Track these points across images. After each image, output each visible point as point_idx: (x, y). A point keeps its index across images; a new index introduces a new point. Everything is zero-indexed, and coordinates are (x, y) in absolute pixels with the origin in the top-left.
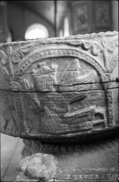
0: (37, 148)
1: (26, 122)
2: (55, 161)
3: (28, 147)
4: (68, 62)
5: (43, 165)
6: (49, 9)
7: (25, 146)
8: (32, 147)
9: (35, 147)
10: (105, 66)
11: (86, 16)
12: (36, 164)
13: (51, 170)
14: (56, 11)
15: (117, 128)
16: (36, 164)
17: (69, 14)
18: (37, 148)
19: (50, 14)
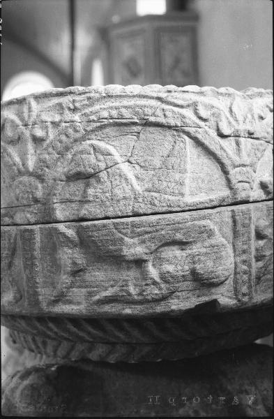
6: (58, 39)
14: (73, 47)
17: (103, 53)
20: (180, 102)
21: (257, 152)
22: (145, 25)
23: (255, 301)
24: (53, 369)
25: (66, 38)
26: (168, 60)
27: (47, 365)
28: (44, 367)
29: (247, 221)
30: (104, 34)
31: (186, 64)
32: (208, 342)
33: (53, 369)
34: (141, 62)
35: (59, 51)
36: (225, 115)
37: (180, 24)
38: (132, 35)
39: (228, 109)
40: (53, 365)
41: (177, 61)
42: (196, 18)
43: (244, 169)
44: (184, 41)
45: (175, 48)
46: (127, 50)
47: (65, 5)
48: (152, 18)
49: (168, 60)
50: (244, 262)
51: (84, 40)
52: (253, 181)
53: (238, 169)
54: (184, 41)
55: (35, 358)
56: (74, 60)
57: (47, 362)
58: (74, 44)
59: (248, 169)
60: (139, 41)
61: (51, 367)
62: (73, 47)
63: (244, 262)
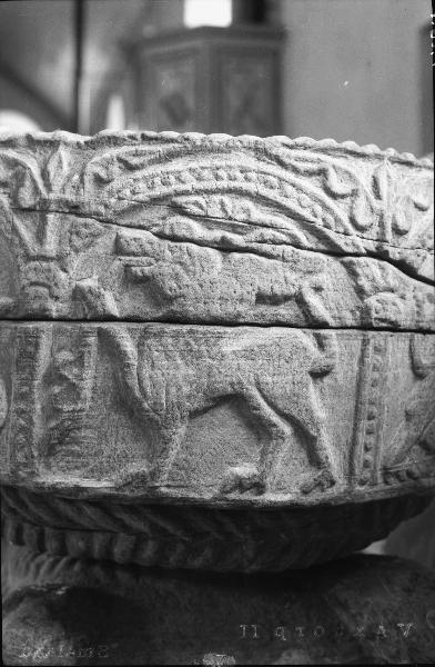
0: (28, 568)
6: (53, 60)
14: (78, 73)
17: (127, 86)
18: (28, 568)
20: (302, 166)
21: (74, 237)
22: (198, 43)
23: (40, 480)
24: (60, 593)
25: (66, 60)
26: (234, 100)
27: (48, 585)
28: (45, 590)
29: (31, 349)
30: (134, 58)
31: (262, 107)
32: (301, 556)
33: (60, 593)
34: (190, 101)
35: (57, 79)
36: (34, 181)
37: (258, 43)
38: (176, 58)
39: (371, 180)
40: (59, 587)
41: (248, 103)
42: (280, 35)
43: (44, 264)
44: (261, 72)
45: (246, 80)
46: (168, 82)
47: (68, 8)
48: (208, 32)
49: (234, 100)
50: (21, 413)
51: (97, 63)
52: (56, 284)
53: (33, 264)
54: (261, 72)
55: (26, 573)
56: (80, 101)
57: (47, 581)
58: (76, 68)
59: (53, 265)
60: (188, 68)
61: (56, 590)
62: (78, 73)
63: (21, 413)
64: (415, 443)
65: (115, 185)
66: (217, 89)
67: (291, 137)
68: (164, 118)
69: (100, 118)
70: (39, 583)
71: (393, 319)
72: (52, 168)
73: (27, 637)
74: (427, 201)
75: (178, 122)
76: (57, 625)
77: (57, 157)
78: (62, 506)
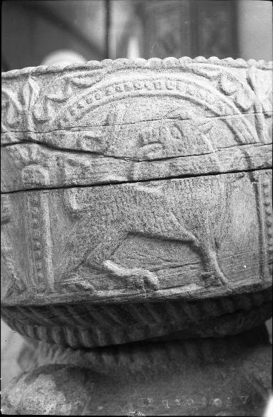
0: (48, 351)
1: (236, 222)
2: (88, 383)
3: (31, 346)
4: (28, 197)
5: (58, 393)
6: (92, 16)
7: (26, 343)
8: (40, 347)
9: (45, 349)
10: (259, 137)
11: (178, 38)
12: (42, 391)
13: (78, 404)
14: (108, 23)
15: (264, 292)
16: (42, 391)
17: (138, 31)
18: (48, 351)
19: (95, 30)
26: (206, 35)
31: (224, 40)
41: (215, 37)
44: (223, 16)
49: (206, 35)
55: (47, 356)
64: (144, 278)
65: (71, 102)
66: (195, 28)
67: (246, 59)
68: (162, 51)
69: (123, 52)
70: (131, 396)
71: (38, 182)
72: (26, 91)
73: (39, 402)
74: (270, 113)
75: (170, 53)
76: (61, 394)
77: (27, 85)
78: (56, 312)
